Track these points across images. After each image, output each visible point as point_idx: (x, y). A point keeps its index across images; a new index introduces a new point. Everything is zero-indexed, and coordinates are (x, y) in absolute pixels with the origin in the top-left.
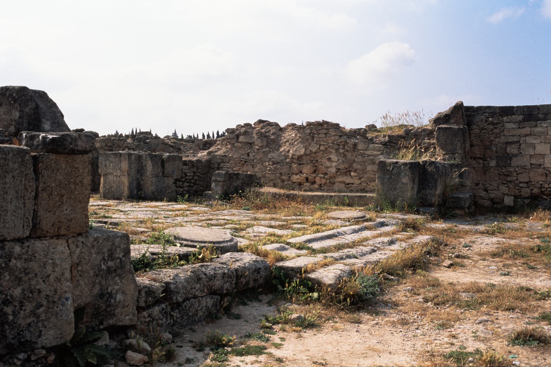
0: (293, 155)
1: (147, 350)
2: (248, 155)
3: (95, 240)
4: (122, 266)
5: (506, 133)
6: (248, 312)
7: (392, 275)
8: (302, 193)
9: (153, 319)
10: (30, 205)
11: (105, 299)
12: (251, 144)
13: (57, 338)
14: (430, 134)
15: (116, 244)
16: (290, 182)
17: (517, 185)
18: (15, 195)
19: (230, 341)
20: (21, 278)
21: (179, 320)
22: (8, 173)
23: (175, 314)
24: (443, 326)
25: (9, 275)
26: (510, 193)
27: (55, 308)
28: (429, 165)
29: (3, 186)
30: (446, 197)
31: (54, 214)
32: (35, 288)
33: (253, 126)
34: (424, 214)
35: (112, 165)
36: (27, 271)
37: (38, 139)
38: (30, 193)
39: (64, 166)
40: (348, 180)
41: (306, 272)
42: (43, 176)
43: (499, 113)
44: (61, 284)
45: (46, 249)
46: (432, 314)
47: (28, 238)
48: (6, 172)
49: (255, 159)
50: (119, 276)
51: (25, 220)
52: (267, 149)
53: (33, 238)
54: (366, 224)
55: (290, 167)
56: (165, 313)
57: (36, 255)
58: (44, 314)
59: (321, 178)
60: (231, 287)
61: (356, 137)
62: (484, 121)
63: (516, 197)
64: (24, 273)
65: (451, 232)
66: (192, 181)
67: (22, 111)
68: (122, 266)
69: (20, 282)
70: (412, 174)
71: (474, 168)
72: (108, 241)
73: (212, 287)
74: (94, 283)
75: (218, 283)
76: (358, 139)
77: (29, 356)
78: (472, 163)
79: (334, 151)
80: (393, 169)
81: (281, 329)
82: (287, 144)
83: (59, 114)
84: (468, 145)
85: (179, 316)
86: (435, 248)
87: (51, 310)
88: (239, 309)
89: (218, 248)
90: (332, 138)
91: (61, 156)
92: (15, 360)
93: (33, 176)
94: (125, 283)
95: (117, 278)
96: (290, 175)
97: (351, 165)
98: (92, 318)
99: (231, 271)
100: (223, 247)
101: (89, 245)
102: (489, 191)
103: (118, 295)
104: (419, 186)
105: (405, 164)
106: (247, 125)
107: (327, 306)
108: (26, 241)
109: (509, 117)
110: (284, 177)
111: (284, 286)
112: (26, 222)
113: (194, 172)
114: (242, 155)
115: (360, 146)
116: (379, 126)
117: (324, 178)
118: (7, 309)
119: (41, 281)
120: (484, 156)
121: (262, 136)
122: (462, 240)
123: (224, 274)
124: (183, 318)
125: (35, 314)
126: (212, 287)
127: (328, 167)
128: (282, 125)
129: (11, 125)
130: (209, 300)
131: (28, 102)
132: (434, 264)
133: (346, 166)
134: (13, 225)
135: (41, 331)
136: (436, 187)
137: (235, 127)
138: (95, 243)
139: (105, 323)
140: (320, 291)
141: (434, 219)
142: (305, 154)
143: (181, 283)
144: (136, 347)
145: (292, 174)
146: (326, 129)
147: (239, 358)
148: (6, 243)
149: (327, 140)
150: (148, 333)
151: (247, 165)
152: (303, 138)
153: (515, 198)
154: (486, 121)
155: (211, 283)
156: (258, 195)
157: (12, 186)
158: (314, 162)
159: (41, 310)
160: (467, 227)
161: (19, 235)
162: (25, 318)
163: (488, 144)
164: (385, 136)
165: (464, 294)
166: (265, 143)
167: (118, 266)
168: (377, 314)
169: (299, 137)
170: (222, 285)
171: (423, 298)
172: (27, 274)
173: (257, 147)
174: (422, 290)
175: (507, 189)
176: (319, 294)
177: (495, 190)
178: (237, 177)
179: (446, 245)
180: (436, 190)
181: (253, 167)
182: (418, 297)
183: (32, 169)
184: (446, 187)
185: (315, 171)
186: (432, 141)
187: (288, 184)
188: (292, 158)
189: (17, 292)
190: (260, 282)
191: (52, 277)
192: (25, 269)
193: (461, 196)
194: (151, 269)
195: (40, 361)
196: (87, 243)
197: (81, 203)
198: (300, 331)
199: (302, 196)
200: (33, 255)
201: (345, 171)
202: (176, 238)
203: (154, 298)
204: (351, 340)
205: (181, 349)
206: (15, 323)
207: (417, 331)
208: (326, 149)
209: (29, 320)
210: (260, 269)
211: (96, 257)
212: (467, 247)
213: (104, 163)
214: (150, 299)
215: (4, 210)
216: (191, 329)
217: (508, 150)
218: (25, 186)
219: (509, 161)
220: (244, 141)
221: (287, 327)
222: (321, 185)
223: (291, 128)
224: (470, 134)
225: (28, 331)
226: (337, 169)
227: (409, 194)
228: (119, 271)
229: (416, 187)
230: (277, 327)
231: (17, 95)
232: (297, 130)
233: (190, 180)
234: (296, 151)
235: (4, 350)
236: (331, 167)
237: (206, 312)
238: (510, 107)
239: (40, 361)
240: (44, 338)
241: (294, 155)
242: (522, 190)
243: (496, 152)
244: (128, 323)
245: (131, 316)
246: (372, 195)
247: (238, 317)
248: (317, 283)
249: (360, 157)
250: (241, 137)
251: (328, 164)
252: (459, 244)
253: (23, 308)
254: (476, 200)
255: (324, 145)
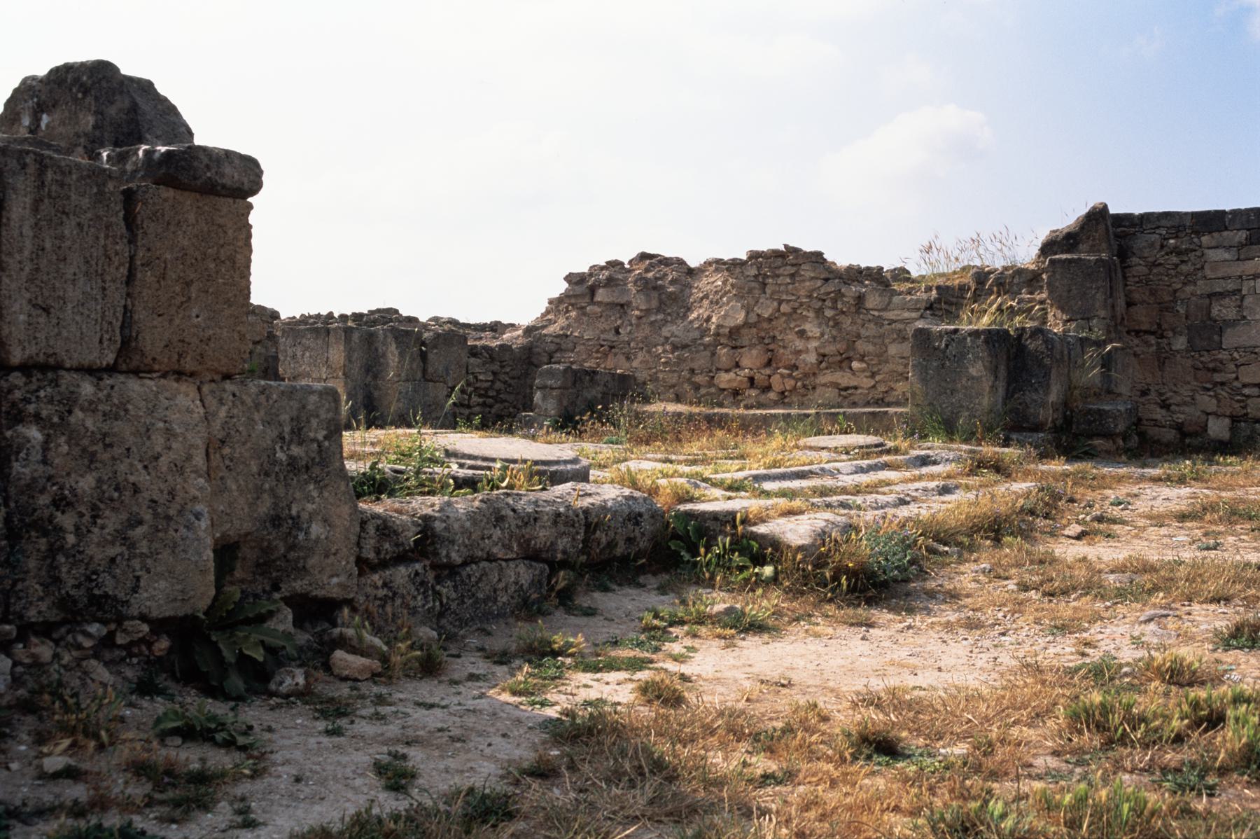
0: (719, 326)
2: (618, 333)
3: (262, 393)
5: (1208, 272)
6: (614, 605)
7: (945, 545)
8: (741, 411)
9: (395, 594)
11: (284, 529)
12: (622, 306)
13: (175, 600)
16: (713, 390)
17: (1237, 391)
18: (84, 268)
19: (571, 645)
20: (93, 454)
21: (454, 606)
23: (445, 591)
25: (68, 443)
26: (1220, 411)
27: (172, 532)
28: (1030, 337)
29: (57, 242)
30: (1072, 411)
31: (171, 321)
33: (627, 266)
34: (1021, 444)
36: (108, 440)
37: (134, 159)
38: (117, 269)
39: (191, 217)
40: (844, 379)
42: (145, 233)
44: (185, 481)
45: (152, 396)
46: (1037, 610)
50: (317, 482)
51: (105, 326)
52: (660, 317)
53: (121, 372)
54: (885, 458)
55: (713, 354)
56: (422, 583)
57: (130, 407)
58: (145, 542)
59: (782, 376)
60: (573, 547)
61: (862, 283)
62: (1158, 245)
63: (1234, 419)
64: (101, 445)
65: (1082, 478)
66: (491, 393)
67: (102, 114)
69: (91, 462)
70: (990, 355)
71: (1135, 355)
72: (290, 399)
74: (259, 490)
75: (543, 535)
76: (866, 286)
77: (111, 635)
79: (811, 314)
80: (947, 346)
81: (687, 634)
82: (706, 302)
83: (183, 129)
84: (1121, 302)
85: (454, 595)
86: (1047, 504)
87: (160, 534)
88: (592, 599)
90: (808, 284)
91: (187, 194)
92: (80, 638)
93: (124, 230)
94: (331, 500)
95: (312, 487)
96: (712, 373)
97: (851, 345)
98: (254, 573)
100: (556, 472)
101: (249, 401)
102: (1173, 408)
103: (314, 526)
104: (1009, 384)
105: (976, 334)
106: (614, 264)
107: (793, 594)
108: (105, 376)
109: (1215, 235)
110: (698, 379)
112: (107, 332)
113: (494, 373)
114: (603, 331)
115: (873, 301)
116: (914, 274)
118: (64, 517)
119: (140, 466)
120: (1159, 326)
121: (648, 286)
122: (1108, 492)
123: (558, 515)
124: (463, 602)
125: (124, 539)
126: (529, 540)
127: (799, 352)
128: (693, 262)
129: (76, 145)
130: (522, 569)
133: (841, 346)
134: (78, 334)
135: (138, 578)
136: (1048, 386)
137: (586, 270)
138: (262, 398)
140: (779, 561)
141: (1044, 456)
142: (746, 324)
143: (458, 520)
144: (355, 642)
145: (718, 369)
146: (793, 265)
147: (589, 675)
148: (63, 373)
149: (796, 289)
150: (382, 623)
151: (615, 355)
154: (1162, 247)
155: (527, 531)
156: (639, 417)
157: (77, 246)
158: (766, 341)
159: (140, 530)
160: (1123, 471)
161: (92, 358)
162: (103, 544)
163: (1167, 298)
164: (929, 289)
165: (1112, 577)
166: (654, 304)
167: (313, 459)
168: (911, 611)
169: (732, 285)
170: (552, 539)
171: (1018, 584)
173: (637, 313)
174: (1014, 571)
175: (1214, 401)
176: (776, 568)
177: (1185, 404)
178: (592, 380)
179: (1072, 500)
180: (1047, 393)
181: (628, 358)
182: (1006, 583)
183: (121, 214)
184: (1071, 388)
187: (708, 394)
188: (717, 334)
189: (86, 484)
190: (642, 545)
192: (105, 435)
193: (1107, 408)
194: (391, 494)
195: (135, 650)
196: (244, 397)
197: (230, 306)
198: (733, 637)
199: (740, 417)
200: (123, 406)
201: (839, 358)
203: (397, 545)
204: (848, 652)
206: (79, 552)
207: (1003, 638)
208: (795, 310)
209: (112, 551)
210: (640, 515)
211: (264, 432)
212: (1120, 504)
213: (290, 352)
214: (387, 546)
215: (59, 297)
216: (483, 630)
217: (1215, 312)
219: (1216, 338)
220: (607, 300)
221: (703, 630)
222: (783, 393)
223: (712, 269)
224: (1125, 277)
225: (110, 573)
228: (316, 471)
230: (675, 631)
233: (486, 390)
235: (55, 611)
236: (807, 351)
237: (516, 595)
238: (1217, 212)
239: (135, 650)
240: (145, 595)
241: (722, 326)
242: (1249, 401)
243: (1187, 318)
244: (335, 593)
245: (343, 579)
246: (899, 410)
247: (590, 612)
248: (771, 546)
249: (872, 325)
250: (601, 291)
251: (799, 344)
252: (1102, 500)
253: (99, 521)
254: (1143, 428)
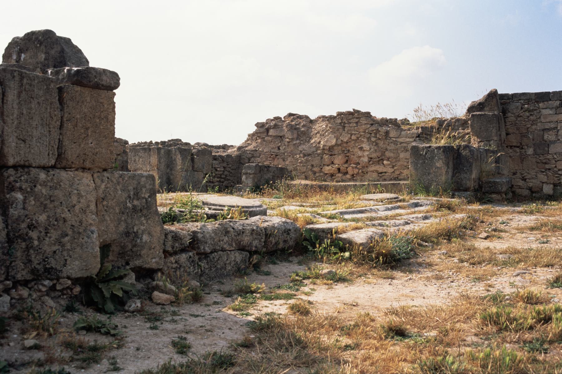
0: (324, 146)
1: (173, 291)
2: (279, 149)
4: (148, 207)
7: (426, 242)
8: (334, 183)
9: (181, 266)
10: (56, 134)
11: (131, 238)
12: (281, 137)
13: (83, 269)
14: (463, 123)
15: (142, 183)
16: (322, 174)
17: (556, 173)
18: (40, 122)
19: (259, 288)
21: (207, 271)
22: (33, 98)
23: (203, 264)
24: (479, 279)
25: (34, 200)
27: (81, 239)
29: (29, 111)
30: (482, 182)
31: (80, 145)
32: (60, 216)
33: (283, 119)
34: (460, 197)
35: (141, 160)
36: (52, 199)
37: (63, 73)
39: (88, 99)
40: (380, 168)
41: (336, 232)
42: (68, 106)
43: (535, 100)
44: (87, 217)
46: (467, 271)
47: (54, 167)
48: (32, 97)
49: (286, 152)
52: (298, 142)
53: (58, 168)
54: (399, 204)
55: (322, 158)
56: (193, 261)
57: (62, 184)
59: (353, 168)
60: (260, 244)
61: (388, 126)
62: (520, 108)
63: (555, 185)
64: (49, 200)
65: (487, 212)
66: (223, 176)
67: (48, 53)
68: (148, 207)
69: (45, 208)
70: (445, 157)
71: (510, 157)
72: (133, 179)
73: (240, 242)
74: (120, 220)
75: (246, 239)
77: (54, 285)
78: (508, 152)
79: (365, 140)
80: (426, 153)
81: (311, 283)
82: (318, 135)
83: (84, 60)
84: (504, 133)
85: (207, 267)
86: (471, 224)
87: (76, 240)
88: (269, 267)
89: (245, 212)
90: (364, 126)
91: (87, 88)
92: (41, 287)
93: (58, 105)
94: (152, 224)
95: (143, 219)
97: (383, 154)
99: (260, 229)
100: (252, 211)
101: (115, 181)
102: (527, 180)
104: (454, 170)
105: (439, 148)
107: (359, 264)
109: (546, 103)
110: (315, 169)
111: (314, 247)
112: (51, 150)
113: (224, 168)
114: (273, 148)
115: (393, 134)
116: (411, 121)
117: (356, 167)
119: (66, 210)
120: (521, 144)
121: (292, 128)
122: (498, 218)
123: (253, 230)
124: (211, 270)
126: (240, 242)
127: (360, 157)
128: (312, 117)
129: (37, 68)
130: (237, 254)
131: (53, 45)
132: (469, 236)
133: (379, 154)
134: (38, 151)
135: (66, 260)
136: (471, 171)
137: (264, 121)
138: (121, 180)
139: (131, 263)
140: (352, 250)
141: (470, 202)
142: (336, 145)
143: (208, 233)
144: (163, 288)
145: (324, 165)
146: (357, 118)
147: (268, 302)
149: (358, 129)
150: (175, 279)
151: (278, 159)
152: (334, 128)
153: (554, 186)
154: (522, 108)
155: (239, 238)
157: (37, 112)
158: (345, 152)
159: (67, 239)
160: (505, 208)
162: (50, 245)
164: (418, 128)
165: (501, 256)
167: (144, 206)
168: (411, 272)
169: (330, 127)
170: (251, 241)
171: (459, 260)
172: (52, 201)
173: (287, 140)
174: (457, 254)
176: (350, 253)
177: (533, 178)
178: (268, 170)
179: (482, 222)
180: (471, 174)
181: (284, 160)
182: (453, 259)
183: (57, 98)
185: (347, 161)
186: (466, 131)
187: (319, 176)
188: (323, 149)
189: (42, 218)
191: (77, 208)
192: (51, 196)
193: (497, 180)
195: (65, 292)
196: (113, 179)
197: (106, 138)
198: (331, 284)
200: (59, 183)
201: (378, 159)
202: (204, 203)
203: (181, 244)
205: (209, 295)
207: (452, 284)
208: (358, 138)
209: (54, 248)
210: (290, 230)
212: (504, 223)
213: (133, 159)
214: (177, 245)
216: (220, 282)
217: (546, 137)
218: (50, 114)
219: (546, 149)
220: (274, 134)
221: (318, 281)
222: (353, 175)
226: (369, 158)
227: (443, 178)
228: (145, 212)
229: (450, 171)
231: (43, 37)
232: (328, 120)
233: (221, 175)
234: (327, 141)
235: (29, 275)
236: (364, 156)
238: (546, 93)
239: (65, 292)
240: (69, 267)
241: (326, 146)
243: (533, 140)
244: (154, 266)
245: (157, 259)
247: (268, 274)
249: (392, 145)
250: (271, 130)
251: (360, 153)
252: (496, 221)
253: (48, 235)
255: (355, 134)
